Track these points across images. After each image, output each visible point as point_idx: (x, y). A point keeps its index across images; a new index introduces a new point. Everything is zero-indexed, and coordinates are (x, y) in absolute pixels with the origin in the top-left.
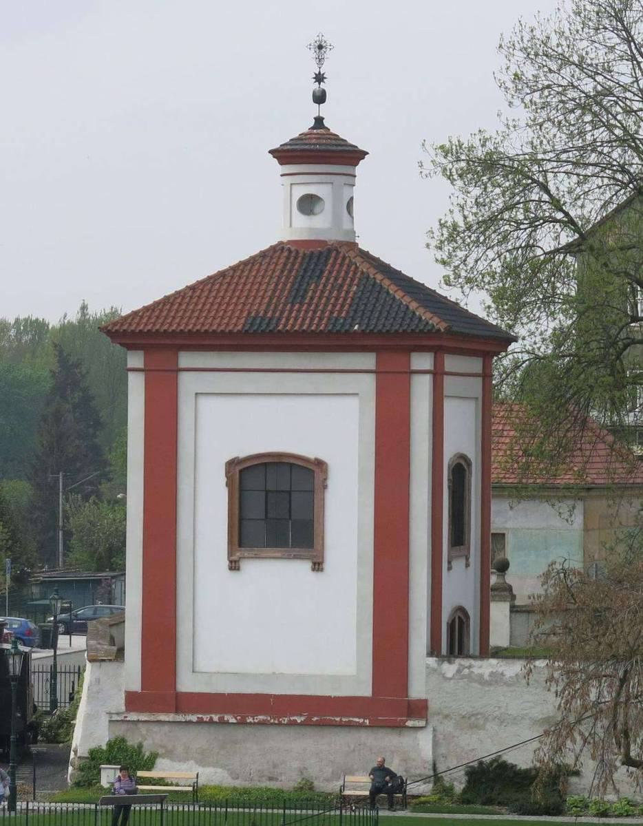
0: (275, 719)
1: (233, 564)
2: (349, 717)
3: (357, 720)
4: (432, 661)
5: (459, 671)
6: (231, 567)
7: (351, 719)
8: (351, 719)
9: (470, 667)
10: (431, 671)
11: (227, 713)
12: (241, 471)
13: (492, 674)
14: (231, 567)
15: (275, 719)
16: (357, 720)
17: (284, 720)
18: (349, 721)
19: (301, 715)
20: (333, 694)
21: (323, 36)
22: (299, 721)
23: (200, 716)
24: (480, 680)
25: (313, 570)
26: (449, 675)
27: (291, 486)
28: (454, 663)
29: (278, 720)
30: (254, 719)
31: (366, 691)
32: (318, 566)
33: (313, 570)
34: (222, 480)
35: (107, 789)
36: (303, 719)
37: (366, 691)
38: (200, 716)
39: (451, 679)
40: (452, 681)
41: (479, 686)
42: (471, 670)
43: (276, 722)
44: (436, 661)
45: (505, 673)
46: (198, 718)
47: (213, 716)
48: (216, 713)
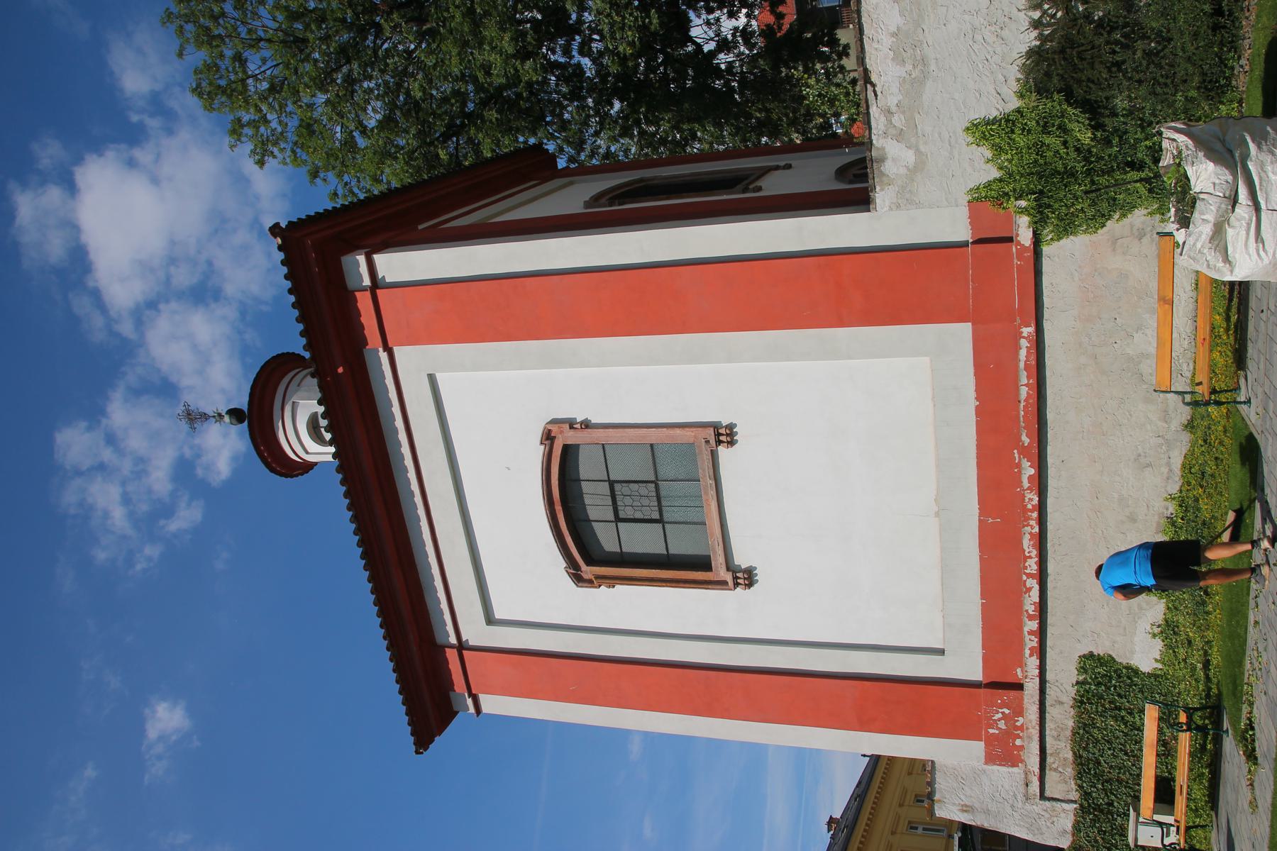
0: (1029, 518)
1: (722, 438)
2: (1017, 366)
3: (1023, 353)
4: (882, 197)
5: (900, 136)
6: (728, 442)
7: (1022, 365)
8: (1022, 365)
9: (888, 112)
10: (907, 200)
11: (1019, 605)
12: (588, 564)
13: (899, 59)
14: (728, 442)
15: (1029, 518)
16: (1023, 353)
17: (1031, 500)
18: (1025, 369)
19: (1019, 465)
20: (970, 402)
21: (189, 405)
22: (1032, 471)
23: (1027, 652)
24: (914, 85)
25: (731, 443)
26: (909, 157)
27: (608, 475)
28: (883, 149)
29: (1032, 511)
30: (1030, 557)
31: (961, 333)
32: (724, 435)
33: (731, 443)
34: (603, 592)
35: (1150, 675)
36: (1026, 464)
37: (961, 333)
38: (1027, 652)
39: (918, 152)
40: (922, 148)
41: (929, 83)
42: (894, 109)
43: (1035, 515)
44: (882, 190)
45: (893, 29)
46: (1031, 655)
47: (1026, 629)
48: (1020, 629)
